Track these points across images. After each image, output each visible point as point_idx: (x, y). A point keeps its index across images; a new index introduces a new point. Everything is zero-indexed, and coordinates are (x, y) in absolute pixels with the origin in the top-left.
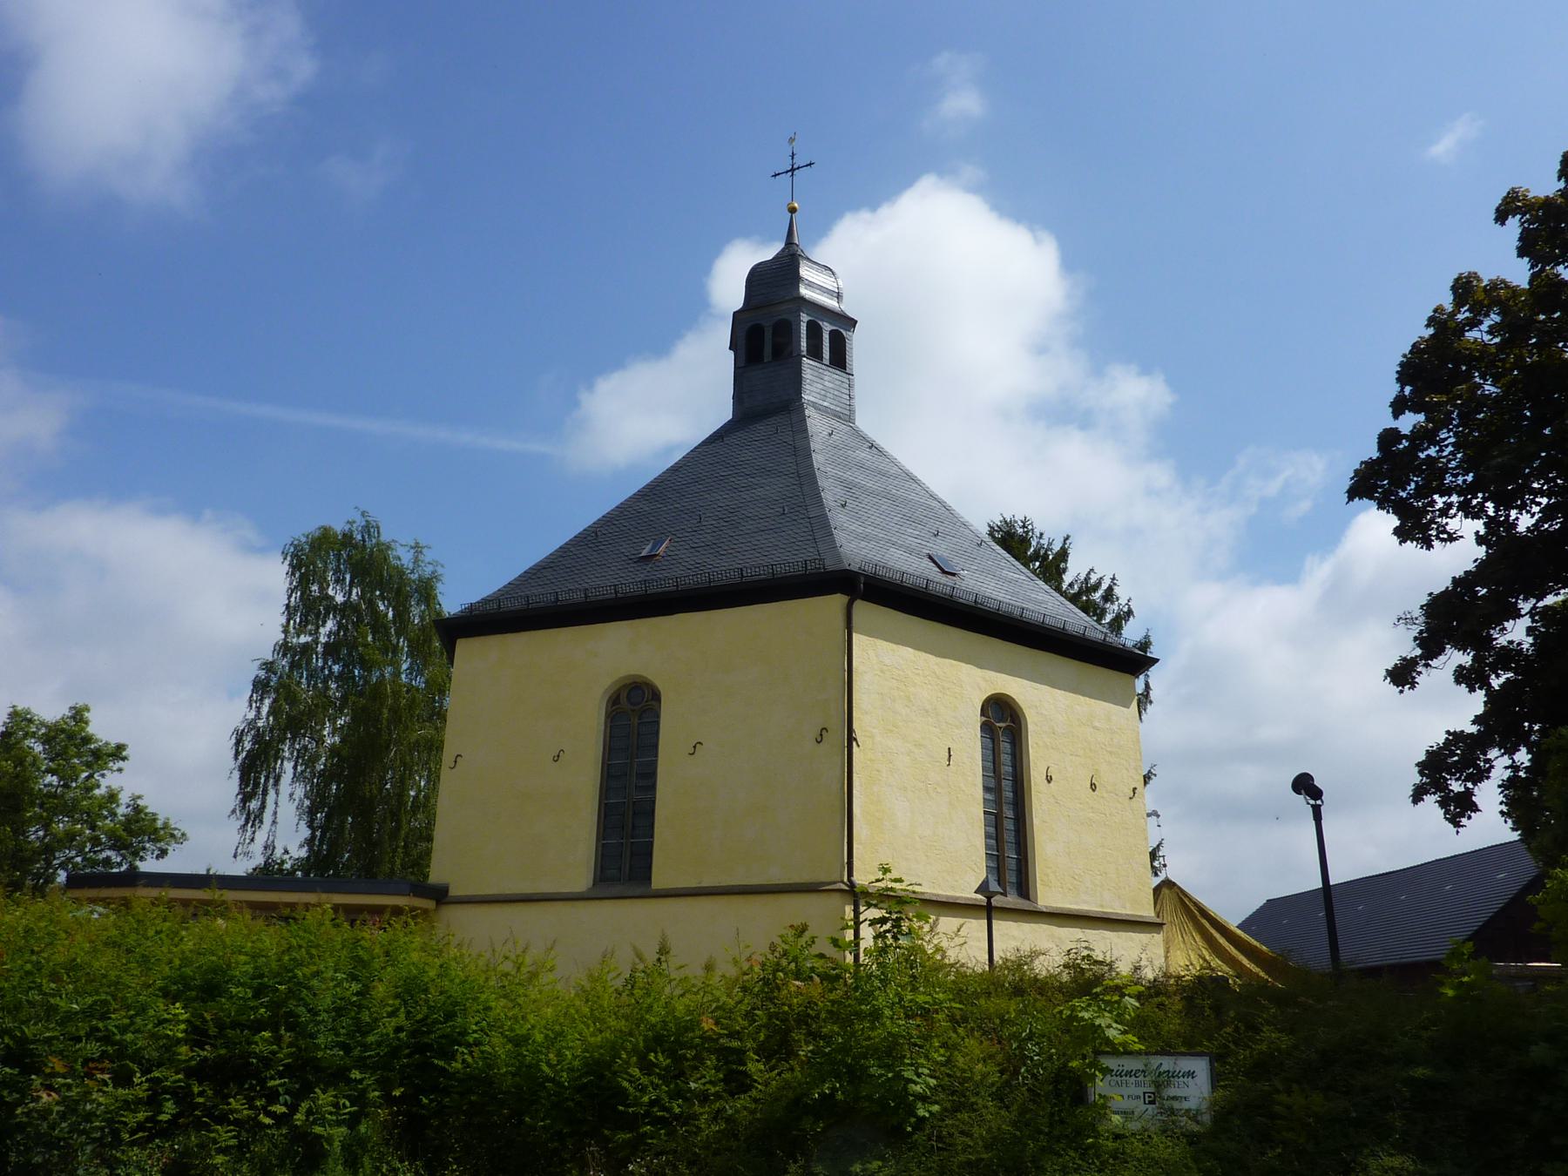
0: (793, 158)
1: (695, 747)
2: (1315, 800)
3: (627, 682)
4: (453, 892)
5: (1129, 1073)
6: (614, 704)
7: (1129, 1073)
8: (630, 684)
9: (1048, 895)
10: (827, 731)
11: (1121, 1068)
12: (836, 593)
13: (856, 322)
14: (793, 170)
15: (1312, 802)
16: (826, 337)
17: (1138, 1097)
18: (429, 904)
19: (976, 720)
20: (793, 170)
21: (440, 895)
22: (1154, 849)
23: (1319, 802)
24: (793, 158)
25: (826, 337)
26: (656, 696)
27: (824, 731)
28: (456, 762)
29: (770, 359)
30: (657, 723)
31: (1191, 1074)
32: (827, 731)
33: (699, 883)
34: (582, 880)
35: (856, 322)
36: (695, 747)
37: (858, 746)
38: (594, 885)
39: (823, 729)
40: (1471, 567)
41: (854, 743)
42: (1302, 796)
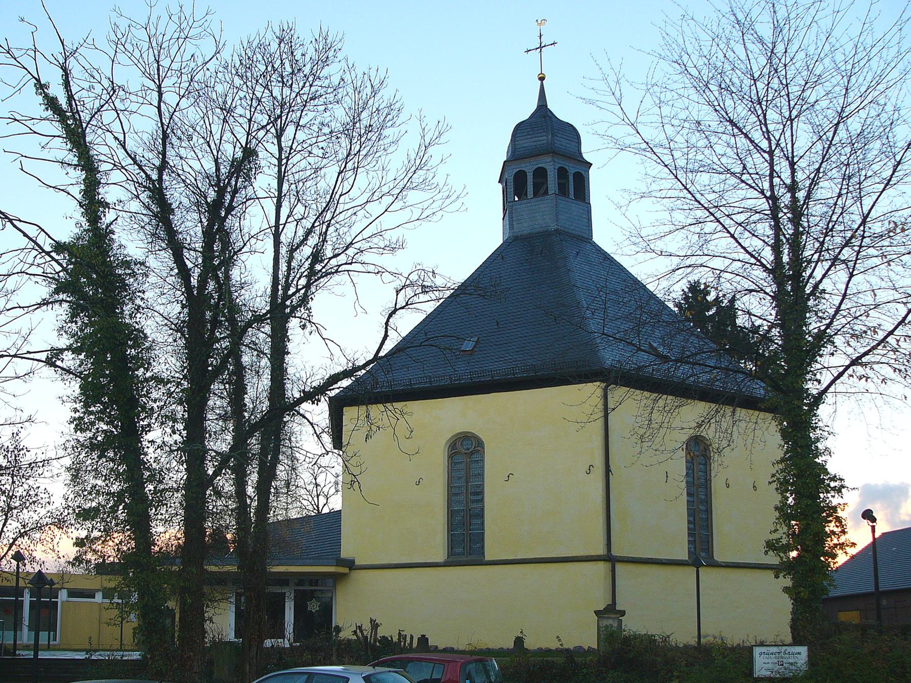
0: (540, 38)
1: (508, 476)
2: (873, 522)
4: (357, 563)
5: (772, 654)
13: (592, 164)
15: (871, 524)
16: (571, 178)
18: (345, 570)
20: (541, 47)
21: (350, 564)
23: (874, 524)
24: (540, 38)
25: (571, 178)
26: (480, 443)
29: (532, 196)
30: (483, 461)
34: (441, 557)
35: (592, 164)
36: (508, 476)
37: (41, 87)
39: (590, 466)
40: (554, 648)
42: (866, 521)
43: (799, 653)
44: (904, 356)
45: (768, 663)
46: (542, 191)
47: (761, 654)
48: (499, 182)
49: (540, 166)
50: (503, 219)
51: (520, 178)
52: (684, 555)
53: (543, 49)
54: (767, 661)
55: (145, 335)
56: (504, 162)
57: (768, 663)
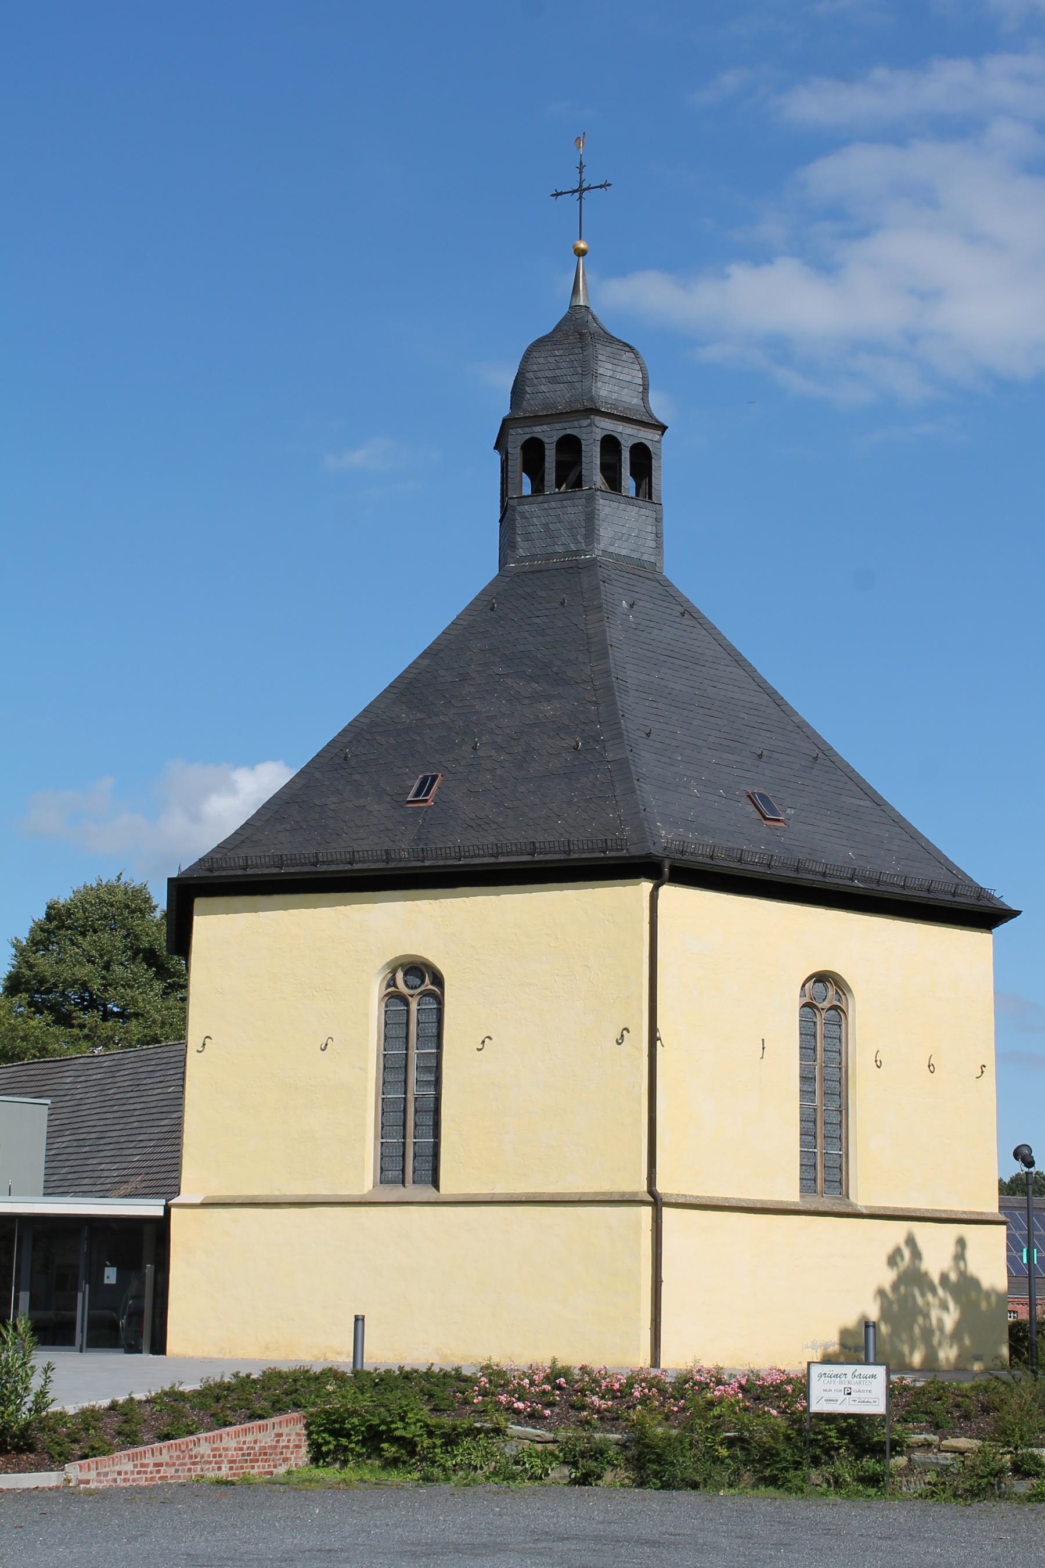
0: (581, 172)
1: (483, 1042)
3: (406, 960)
5: (836, 1376)
6: (388, 986)
7: (836, 1376)
8: (409, 964)
9: (862, 1196)
10: (628, 1032)
11: (831, 1373)
12: (640, 878)
14: (581, 190)
16: (626, 455)
17: (840, 1391)
19: (794, 1002)
20: (581, 190)
22: (580, 1484)
24: (581, 172)
25: (626, 455)
27: (625, 1032)
28: (204, 1044)
31: (874, 1376)
32: (628, 1032)
33: (493, 1189)
36: (483, 1042)
38: (374, 1187)
41: (658, 1042)
43: (874, 1376)
44: (241, 1397)
45: (830, 1390)
46: (572, 477)
47: (820, 1376)
48: (495, 448)
49: (569, 431)
50: (501, 521)
51: (533, 450)
52: (790, 1193)
53: (585, 194)
54: (828, 1387)
55: (307, 1426)
56: (504, 421)
57: (830, 1390)
